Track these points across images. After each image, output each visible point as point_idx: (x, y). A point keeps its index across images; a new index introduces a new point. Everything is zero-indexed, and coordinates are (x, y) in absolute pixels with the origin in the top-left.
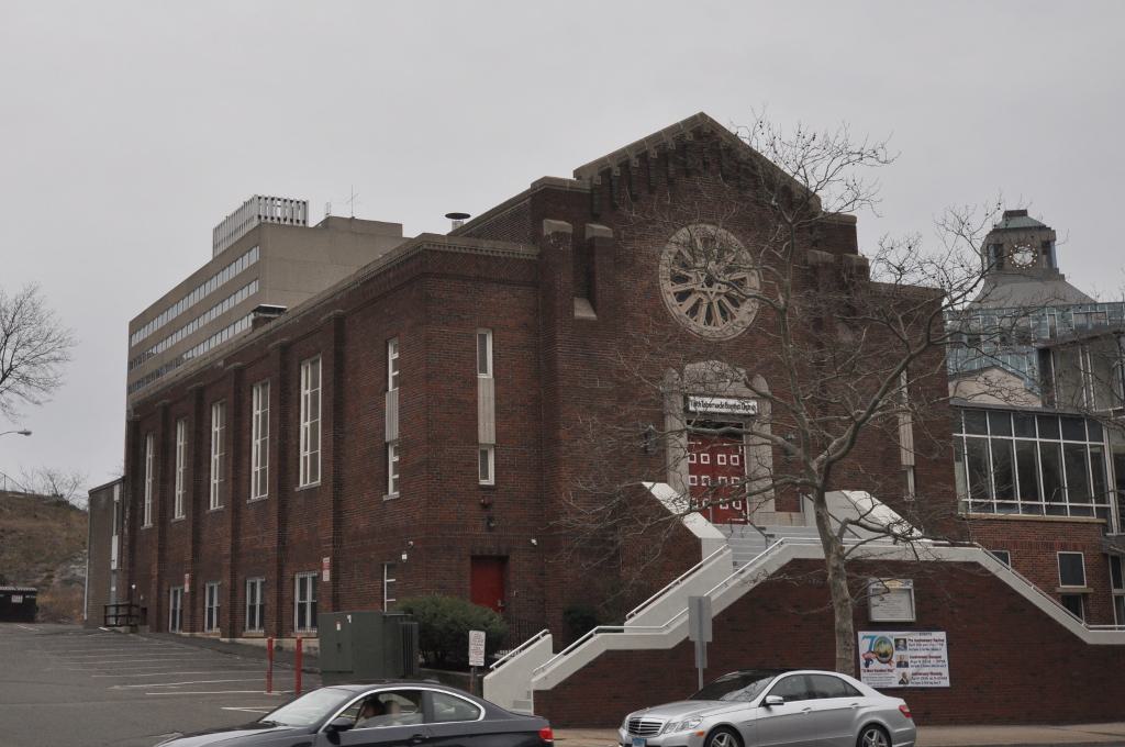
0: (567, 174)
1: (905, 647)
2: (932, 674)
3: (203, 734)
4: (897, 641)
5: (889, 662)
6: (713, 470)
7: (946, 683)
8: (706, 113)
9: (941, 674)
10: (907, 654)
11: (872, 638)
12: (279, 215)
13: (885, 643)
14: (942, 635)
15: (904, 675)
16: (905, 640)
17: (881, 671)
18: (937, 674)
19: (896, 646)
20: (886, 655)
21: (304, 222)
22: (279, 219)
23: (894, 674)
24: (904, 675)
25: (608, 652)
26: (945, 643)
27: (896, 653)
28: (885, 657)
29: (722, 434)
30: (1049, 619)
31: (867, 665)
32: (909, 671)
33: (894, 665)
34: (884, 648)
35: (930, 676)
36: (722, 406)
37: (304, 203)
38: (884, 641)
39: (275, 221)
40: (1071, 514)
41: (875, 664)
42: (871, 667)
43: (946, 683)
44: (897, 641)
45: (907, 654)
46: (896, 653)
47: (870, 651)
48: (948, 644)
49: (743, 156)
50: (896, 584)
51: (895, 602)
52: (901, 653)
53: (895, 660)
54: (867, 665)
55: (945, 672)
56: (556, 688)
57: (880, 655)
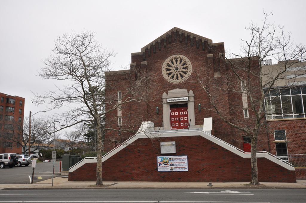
0: (140, 51)
1: (173, 160)
2: (182, 167)
3: (24, 183)
4: (170, 159)
5: (167, 164)
6: (179, 116)
7: (187, 170)
8: (176, 27)
9: (185, 167)
10: (173, 162)
11: (162, 158)
12: (264, 64)
13: (166, 159)
14: (186, 157)
15: (172, 168)
16: (173, 158)
17: (164, 167)
18: (184, 167)
19: (170, 160)
20: (166, 162)
21: (271, 64)
22: (265, 65)
23: (169, 168)
24: (172, 168)
25: (86, 163)
26: (187, 159)
27: (170, 162)
28: (166, 163)
29: (179, 107)
30: (223, 149)
31: (160, 165)
32: (173, 167)
33: (169, 165)
34: (165, 161)
35: (181, 168)
36: (177, 100)
37: (271, 60)
38: (166, 159)
39: (264, 65)
40: (295, 117)
41: (163, 165)
42: (161, 166)
43: (187, 170)
44: (170, 159)
45: (173, 162)
46: (170, 162)
47: (161, 161)
48: (188, 159)
49: (165, 37)
50: (170, 143)
51: (168, 147)
52: (171, 162)
53: (169, 164)
54: (160, 165)
55: (187, 167)
56: (73, 172)
57: (164, 162)
